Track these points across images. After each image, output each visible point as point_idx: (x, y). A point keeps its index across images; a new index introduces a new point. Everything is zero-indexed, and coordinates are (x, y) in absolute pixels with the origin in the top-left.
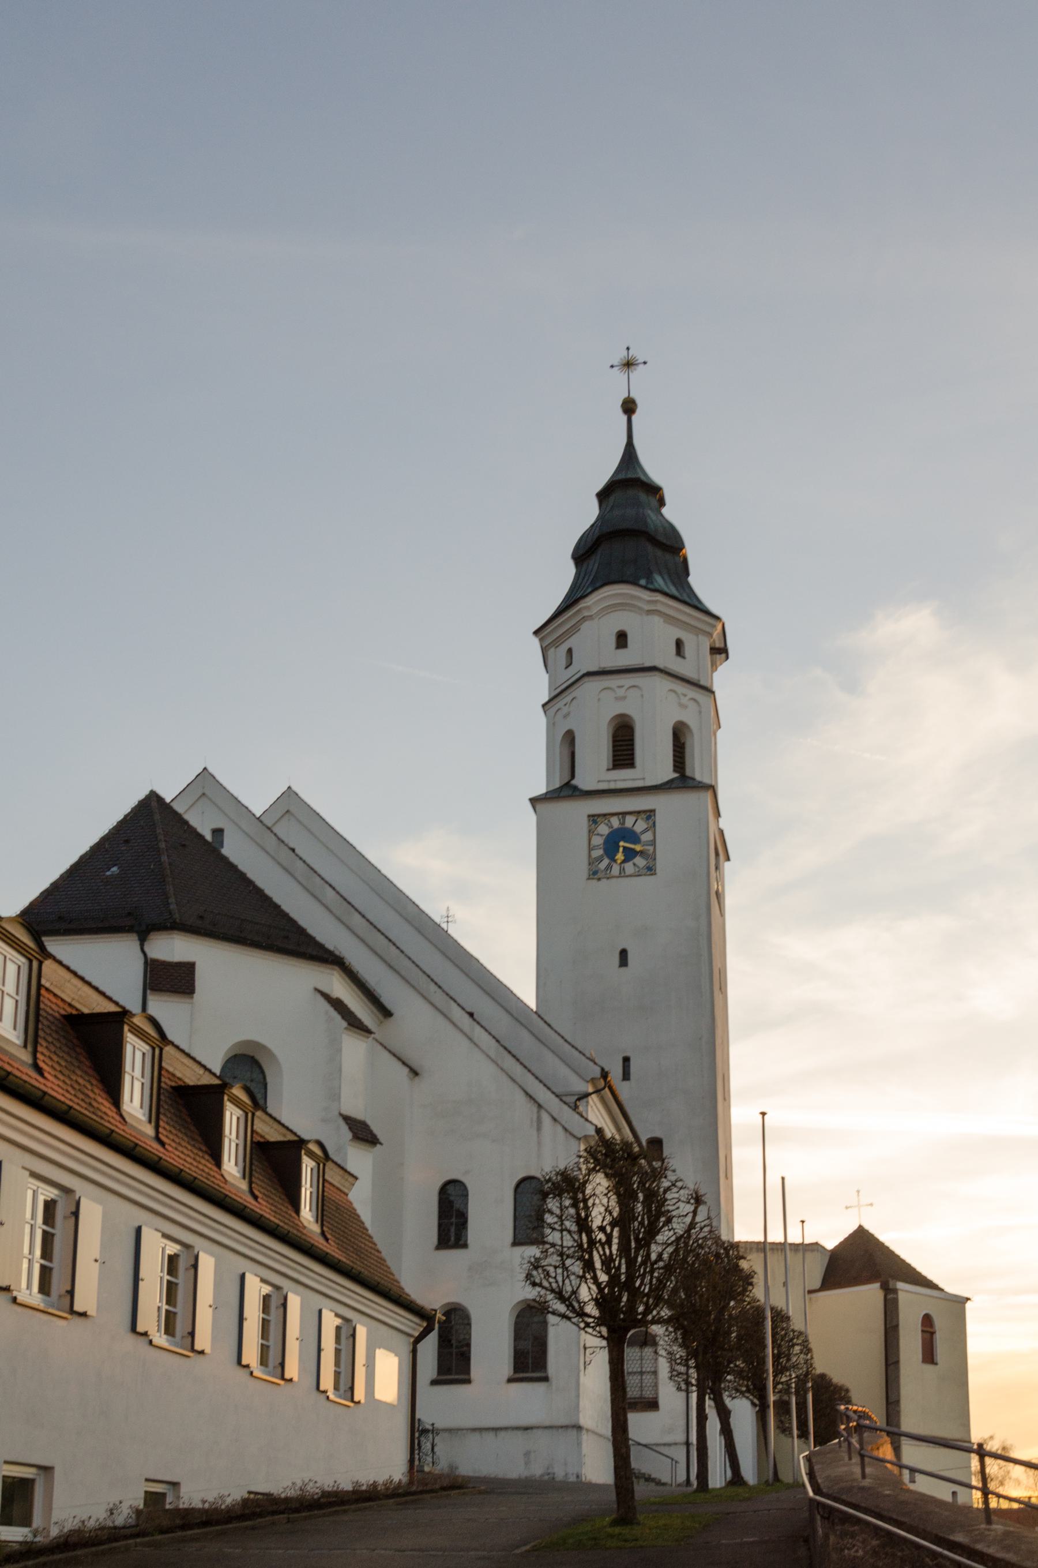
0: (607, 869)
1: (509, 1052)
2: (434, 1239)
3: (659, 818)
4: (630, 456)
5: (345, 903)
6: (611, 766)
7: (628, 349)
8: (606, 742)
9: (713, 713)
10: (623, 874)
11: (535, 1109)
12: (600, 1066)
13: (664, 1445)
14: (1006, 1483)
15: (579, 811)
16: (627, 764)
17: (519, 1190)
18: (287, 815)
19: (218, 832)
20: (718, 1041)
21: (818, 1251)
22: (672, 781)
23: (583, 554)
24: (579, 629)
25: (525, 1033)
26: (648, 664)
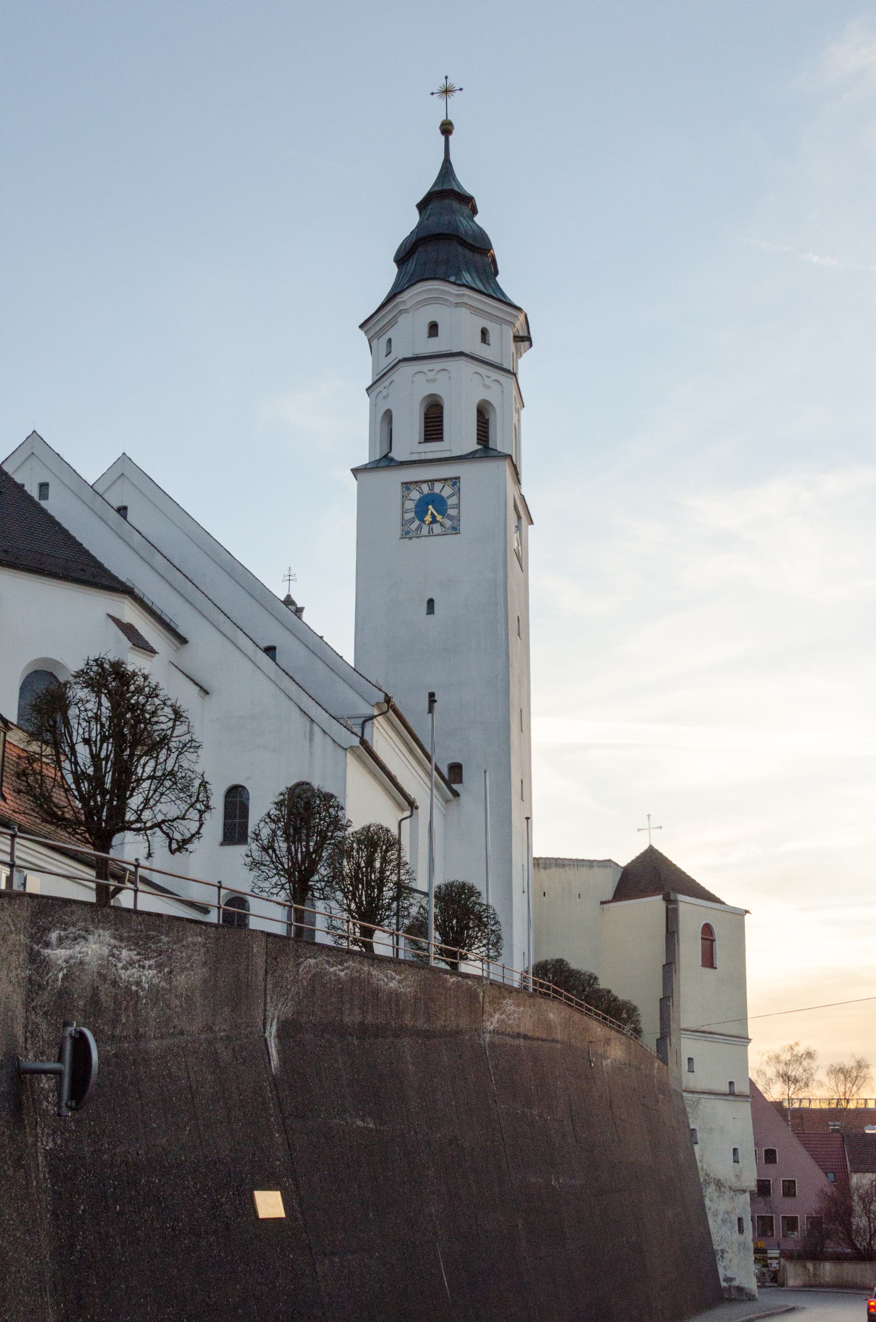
0: (417, 530)
1: (287, 674)
2: (220, 837)
3: (463, 484)
4: (447, 170)
6: (423, 441)
7: (446, 78)
8: (418, 419)
9: (515, 392)
10: (431, 534)
11: (308, 724)
14: (810, 1084)
16: (436, 438)
18: (121, 479)
19: (44, 487)
20: (514, 680)
21: (610, 867)
22: (476, 451)
23: (402, 259)
24: (397, 322)
25: (321, 665)
26: (455, 350)
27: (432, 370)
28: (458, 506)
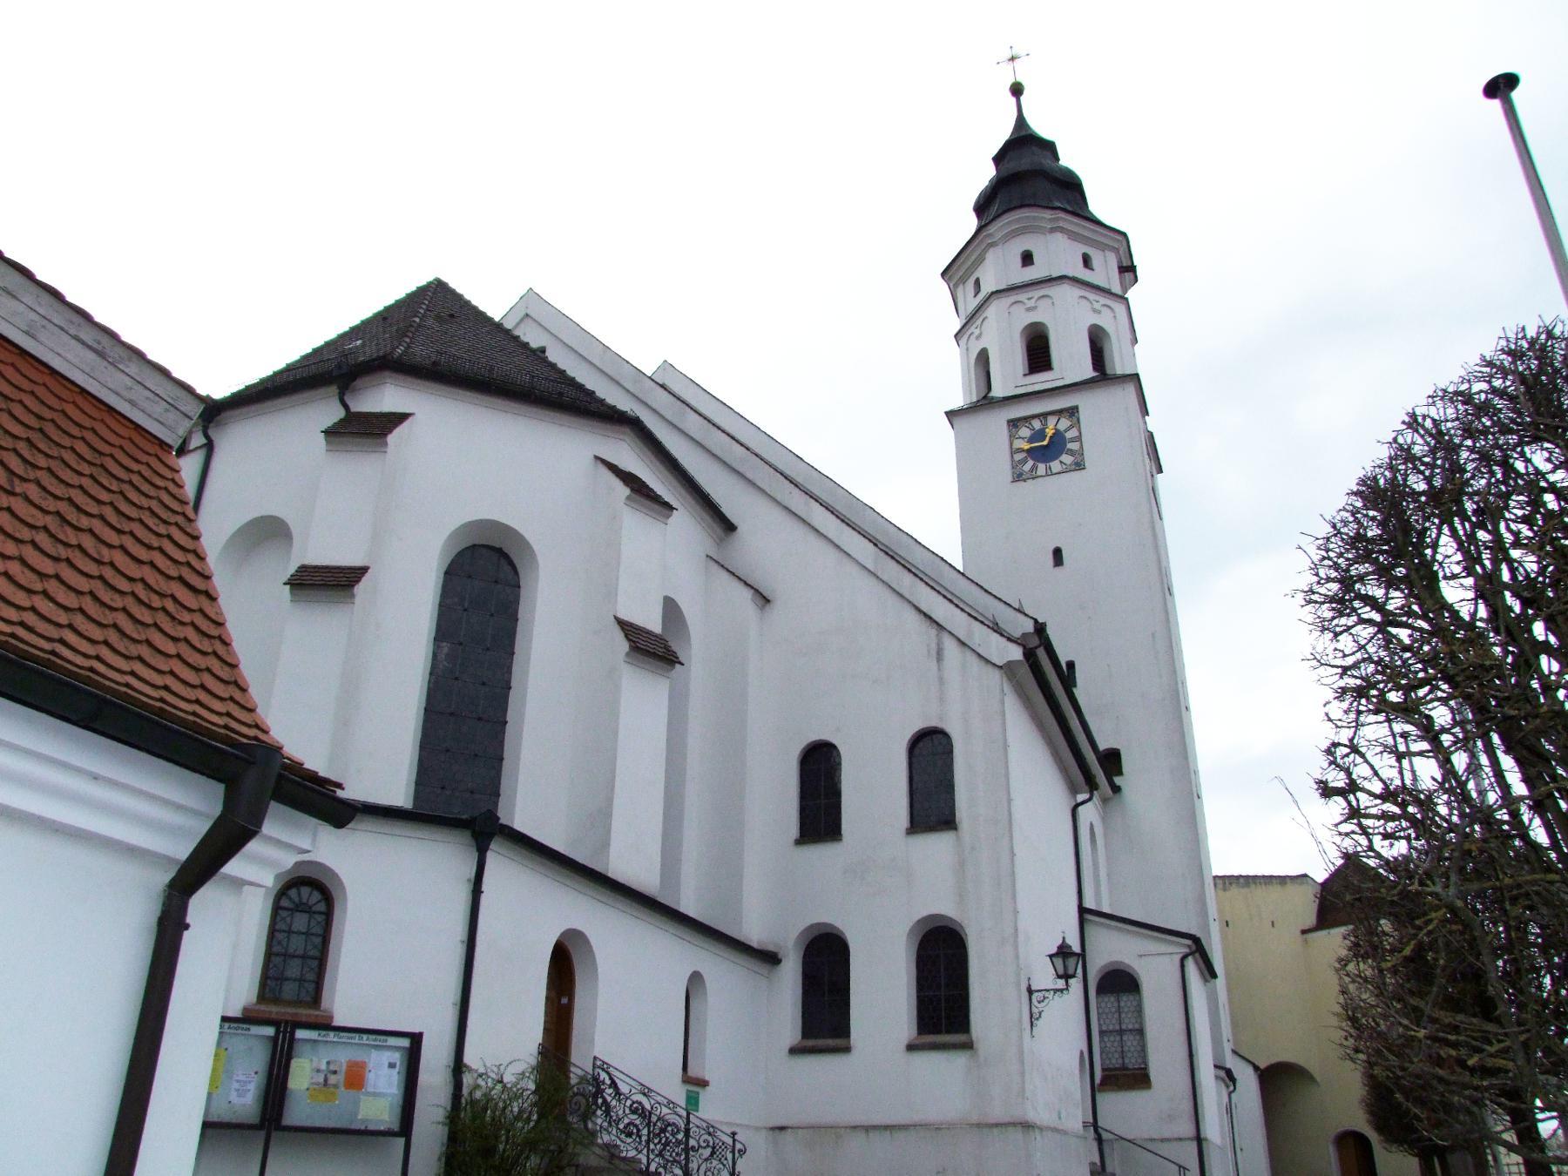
2: (794, 831)
4: (1021, 122)
5: (679, 402)
6: (1027, 372)
12: (1032, 618)
13: (1163, 1140)
15: (996, 422)
17: (917, 751)
23: (984, 206)
27: (1031, 298)
28: (1079, 439)
